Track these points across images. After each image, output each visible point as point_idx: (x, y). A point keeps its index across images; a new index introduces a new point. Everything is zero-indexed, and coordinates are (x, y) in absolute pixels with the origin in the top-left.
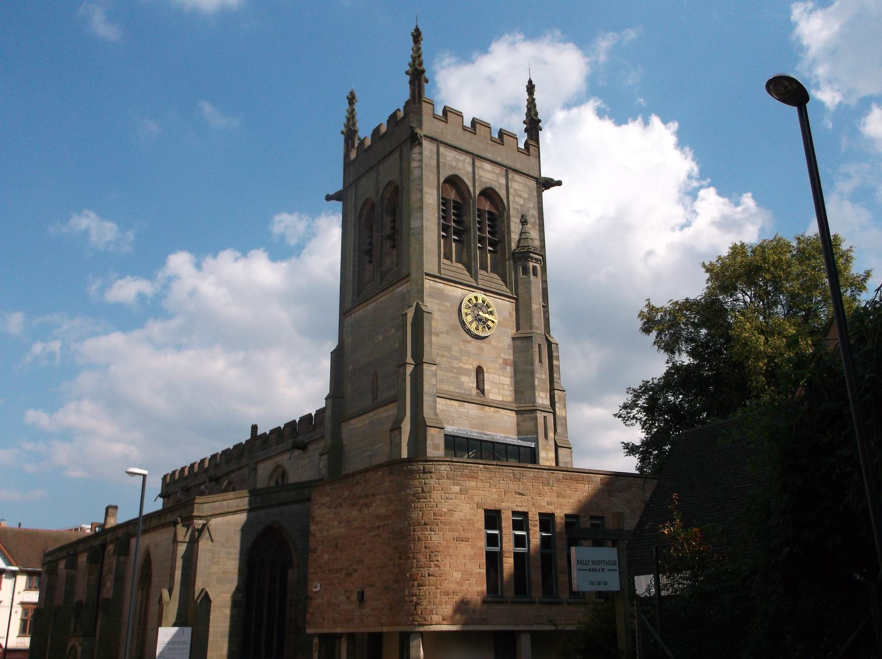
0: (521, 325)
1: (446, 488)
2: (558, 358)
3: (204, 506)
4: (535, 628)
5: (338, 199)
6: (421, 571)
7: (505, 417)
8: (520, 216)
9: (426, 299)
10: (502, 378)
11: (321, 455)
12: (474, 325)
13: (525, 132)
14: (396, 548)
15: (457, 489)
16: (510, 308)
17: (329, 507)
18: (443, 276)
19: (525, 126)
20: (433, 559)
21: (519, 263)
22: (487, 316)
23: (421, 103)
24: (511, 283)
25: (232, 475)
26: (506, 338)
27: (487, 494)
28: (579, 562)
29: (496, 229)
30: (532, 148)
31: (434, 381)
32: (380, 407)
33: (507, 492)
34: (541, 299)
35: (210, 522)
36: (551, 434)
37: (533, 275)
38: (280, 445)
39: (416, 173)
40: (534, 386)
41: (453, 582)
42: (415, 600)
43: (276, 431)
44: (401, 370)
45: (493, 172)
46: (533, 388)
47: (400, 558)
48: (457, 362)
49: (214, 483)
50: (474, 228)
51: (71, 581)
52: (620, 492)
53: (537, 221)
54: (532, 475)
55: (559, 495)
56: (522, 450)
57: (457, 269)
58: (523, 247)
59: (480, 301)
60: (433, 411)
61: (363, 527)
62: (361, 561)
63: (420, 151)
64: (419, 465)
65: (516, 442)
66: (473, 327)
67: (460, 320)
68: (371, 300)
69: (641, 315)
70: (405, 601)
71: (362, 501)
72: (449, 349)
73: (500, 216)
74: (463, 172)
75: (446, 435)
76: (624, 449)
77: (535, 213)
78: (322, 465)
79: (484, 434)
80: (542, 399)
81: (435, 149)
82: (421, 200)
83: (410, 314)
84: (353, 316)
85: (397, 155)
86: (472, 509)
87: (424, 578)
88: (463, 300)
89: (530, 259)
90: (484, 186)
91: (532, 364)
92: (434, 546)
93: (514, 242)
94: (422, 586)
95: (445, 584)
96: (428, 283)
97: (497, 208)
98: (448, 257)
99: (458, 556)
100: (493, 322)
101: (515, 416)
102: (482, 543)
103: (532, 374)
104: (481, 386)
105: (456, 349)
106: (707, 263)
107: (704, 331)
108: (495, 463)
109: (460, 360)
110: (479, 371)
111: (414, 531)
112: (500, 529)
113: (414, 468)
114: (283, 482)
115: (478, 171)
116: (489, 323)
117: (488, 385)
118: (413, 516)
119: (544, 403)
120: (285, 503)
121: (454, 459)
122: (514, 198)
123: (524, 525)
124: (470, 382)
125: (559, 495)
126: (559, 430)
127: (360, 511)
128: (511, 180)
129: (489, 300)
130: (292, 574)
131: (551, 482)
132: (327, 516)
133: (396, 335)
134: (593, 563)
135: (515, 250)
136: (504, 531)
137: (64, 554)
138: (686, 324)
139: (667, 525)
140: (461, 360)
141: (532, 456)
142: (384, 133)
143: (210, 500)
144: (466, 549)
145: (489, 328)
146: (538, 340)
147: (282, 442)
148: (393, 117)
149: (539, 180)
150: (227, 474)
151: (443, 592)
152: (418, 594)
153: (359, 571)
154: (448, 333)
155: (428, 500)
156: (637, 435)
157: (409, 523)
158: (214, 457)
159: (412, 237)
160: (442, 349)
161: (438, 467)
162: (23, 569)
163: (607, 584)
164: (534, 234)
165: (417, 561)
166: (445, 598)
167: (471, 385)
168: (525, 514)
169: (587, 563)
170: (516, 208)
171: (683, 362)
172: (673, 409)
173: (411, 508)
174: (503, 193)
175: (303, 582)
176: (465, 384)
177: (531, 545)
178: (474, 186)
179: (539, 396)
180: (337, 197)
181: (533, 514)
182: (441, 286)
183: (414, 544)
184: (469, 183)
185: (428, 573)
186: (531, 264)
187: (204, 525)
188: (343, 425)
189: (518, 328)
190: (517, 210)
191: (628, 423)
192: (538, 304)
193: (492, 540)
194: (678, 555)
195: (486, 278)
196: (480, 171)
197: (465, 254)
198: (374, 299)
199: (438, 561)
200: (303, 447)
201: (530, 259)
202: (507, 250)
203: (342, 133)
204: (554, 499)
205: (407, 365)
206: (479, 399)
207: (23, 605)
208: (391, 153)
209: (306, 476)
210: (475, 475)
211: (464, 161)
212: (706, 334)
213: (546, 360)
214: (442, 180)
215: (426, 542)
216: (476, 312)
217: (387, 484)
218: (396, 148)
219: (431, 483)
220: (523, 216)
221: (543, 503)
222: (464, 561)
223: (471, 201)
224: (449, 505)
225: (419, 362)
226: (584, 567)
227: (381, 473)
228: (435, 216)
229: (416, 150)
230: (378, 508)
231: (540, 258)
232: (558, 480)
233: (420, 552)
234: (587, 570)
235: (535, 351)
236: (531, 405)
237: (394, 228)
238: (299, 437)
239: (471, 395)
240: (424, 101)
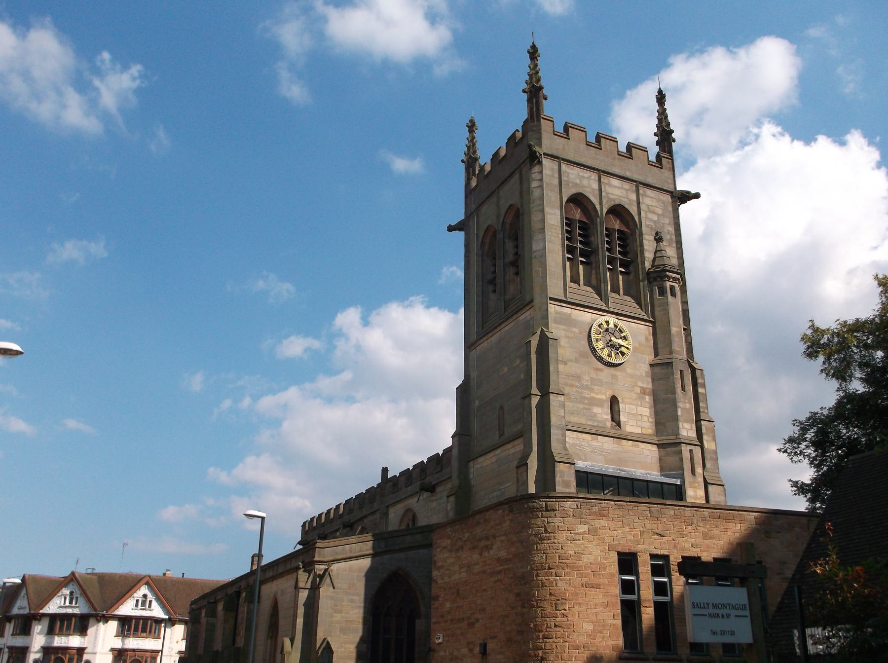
0: (659, 350)
1: (572, 527)
2: (704, 386)
3: (325, 551)
5: (461, 230)
6: (546, 621)
7: (645, 451)
8: (654, 233)
9: (552, 325)
10: (640, 408)
11: (448, 497)
12: (606, 351)
13: (657, 145)
14: (518, 595)
15: (584, 528)
16: (647, 333)
17: (450, 551)
18: (569, 300)
19: (656, 138)
20: (560, 607)
21: (655, 283)
22: (620, 341)
23: (539, 121)
24: (646, 305)
25: (366, 521)
26: (643, 365)
27: (620, 534)
28: (695, 604)
29: (628, 249)
30: (664, 161)
31: (562, 413)
32: (508, 443)
33: (644, 532)
34: (681, 321)
35: (332, 568)
36: (699, 470)
37: (672, 295)
38: (410, 488)
39: (536, 193)
40: (677, 416)
41: (584, 635)
42: (540, 655)
43: (406, 473)
44: (527, 401)
45: (622, 188)
46: (676, 419)
47: (523, 607)
48: (589, 392)
49: (349, 529)
50: (602, 248)
51: (211, 628)
52: (779, 532)
53: (674, 237)
54: (672, 512)
55: (705, 537)
56: (665, 487)
57: (588, 294)
58: (659, 265)
59: (612, 326)
60: (561, 446)
61: (484, 572)
62: (483, 610)
63: (541, 169)
64: (540, 501)
65: (659, 479)
66: (604, 354)
67: (590, 347)
68: (496, 331)
69: (804, 338)
70: (530, 656)
72: (578, 378)
73: (632, 235)
74: (588, 190)
75: (577, 471)
76: (792, 487)
77: (671, 229)
78: (449, 507)
79: (622, 470)
80: (687, 430)
81: (556, 167)
82: (543, 221)
83: (535, 342)
84: (478, 348)
85: (517, 176)
86: (602, 552)
87: (550, 629)
88: (592, 325)
89: (667, 279)
90: (612, 203)
91: (674, 392)
92: (560, 593)
93: (648, 261)
94: (548, 638)
95: (574, 635)
96: (553, 308)
97: (628, 227)
98: (575, 280)
99: (588, 604)
100: (627, 348)
101: (657, 450)
102: (616, 590)
103: (674, 404)
104: (616, 417)
105: (586, 378)
106: (880, 276)
107: (880, 354)
108: (628, 499)
109: (591, 390)
110: (614, 402)
111: (537, 576)
112: (637, 574)
113: (535, 505)
115: (605, 188)
116: (623, 349)
117: (625, 417)
118: (536, 559)
119: (689, 435)
120: (411, 548)
122: (646, 215)
123: (665, 570)
124: (603, 414)
125: (705, 537)
126: (708, 465)
127: (481, 554)
128: (642, 195)
129: (623, 324)
130: (419, 624)
131: (695, 521)
132: (448, 561)
133: (522, 365)
134: (715, 606)
135: (649, 269)
136: (641, 577)
137: (205, 602)
138: (857, 347)
139: (820, 562)
140: (593, 389)
141: (679, 493)
142: (504, 156)
143: (331, 544)
144: (597, 597)
145: (623, 354)
146: (680, 365)
147: (411, 485)
148: (512, 137)
149: (674, 194)
150: (361, 519)
151: (572, 646)
152: (543, 647)
153: (481, 621)
154: (577, 360)
155: (552, 541)
156: (807, 474)
157: (532, 567)
158: (347, 502)
159: (533, 260)
160: (571, 378)
161: (562, 504)
162: (181, 618)
163: (734, 634)
164: (671, 252)
165: (542, 610)
166: (575, 653)
167: (605, 416)
168: (666, 558)
169: (706, 606)
170: (649, 225)
171: (857, 391)
172: (852, 446)
173: (534, 550)
174: (633, 210)
175: (428, 634)
176: (598, 415)
177: (674, 593)
178: (601, 204)
179: (683, 428)
180: (459, 227)
181: (674, 558)
183: (538, 590)
184: (595, 201)
185: (555, 624)
186: (668, 284)
187: (326, 570)
188: (471, 464)
189: (656, 354)
190: (650, 226)
191: (795, 458)
192: (678, 327)
193: (628, 587)
194: (836, 601)
195: (618, 301)
197: (594, 276)
198: (499, 328)
199: (565, 610)
200: (431, 489)
201: (667, 279)
202: (640, 271)
203: (463, 161)
204: (700, 540)
205: (532, 396)
206: (615, 432)
207: (114, 652)
208: (511, 175)
209: (435, 520)
210: (605, 513)
211: (589, 178)
212: (882, 358)
213: (689, 388)
214: (565, 199)
215: (551, 588)
216: (608, 337)
217: (508, 523)
218: (516, 169)
219: (554, 522)
220: (657, 233)
222: (596, 610)
223: (598, 220)
224: (576, 547)
225: (545, 393)
226: (702, 611)
227: (500, 511)
228: (558, 237)
229: (536, 169)
230: (499, 550)
231: (678, 276)
232: (704, 519)
233: (545, 600)
234: (706, 615)
235: (676, 378)
236: (675, 437)
237: (516, 254)
238: (427, 478)
239: (604, 428)
240: (543, 118)
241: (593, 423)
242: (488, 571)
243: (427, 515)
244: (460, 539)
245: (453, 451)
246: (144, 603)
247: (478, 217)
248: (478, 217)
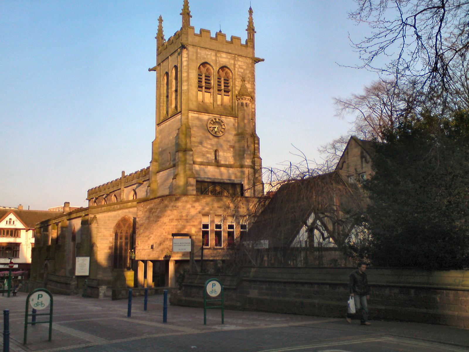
30: (249, 44)
134: (180, 243)
174: (232, 67)
180: (154, 69)
196: (220, 58)
245: (150, 168)
246: (10, 222)
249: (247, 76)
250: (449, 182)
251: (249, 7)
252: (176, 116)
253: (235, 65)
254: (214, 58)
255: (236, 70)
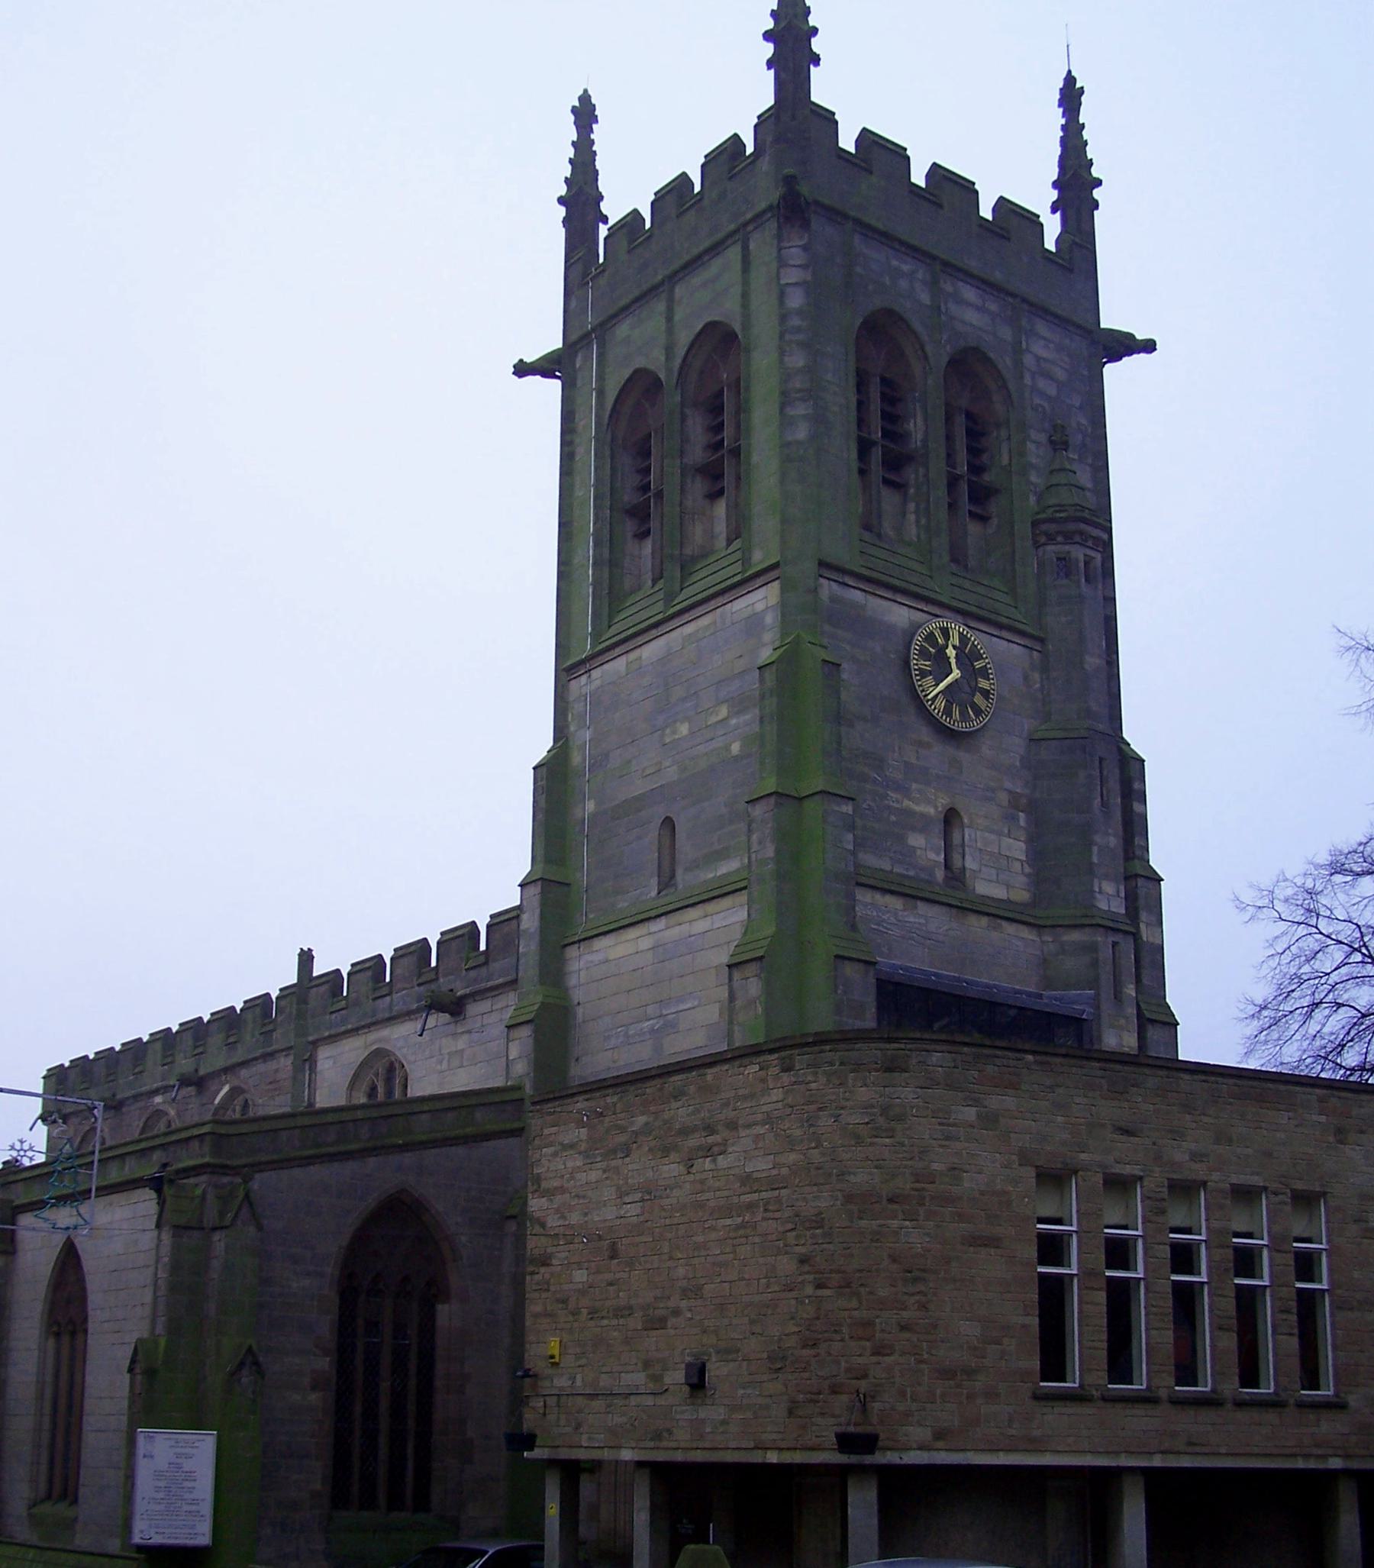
4: (1157, 1462)
5: (547, 374)
10: (1007, 841)
14: (803, 1260)
15: (970, 1113)
25: (244, 1073)
29: (985, 458)
36: (1130, 990)
45: (979, 309)
48: (899, 796)
49: (191, 1090)
52: (1362, 1132)
71: (693, 1141)
78: (514, 1053)
84: (595, 674)
85: (734, 253)
109: (906, 792)
114: (389, 1092)
121: (959, 1038)
133: (734, 721)
145: (978, 712)
167: (932, 856)
174: (1005, 363)
176: (919, 852)
179: (1100, 892)
180: (544, 368)
182: (857, 596)
188: (572, 952)
200: (455, 1008)
208: (715, 249)
217: (777, 1095)
221: (1180, 1156)
241: (907, 869)
242: (712, 1204)
243: (439, 1067)
244: (623, 1130)
245: (525, 917)
247: (602, 346)
248: (602, 346)
249: (1074, 425)
250: (220, 1240)
251: (1067, 69)
252: (720, 600)
253: (1017, 351)
254: (925, 298)
255: (1028, 380)
